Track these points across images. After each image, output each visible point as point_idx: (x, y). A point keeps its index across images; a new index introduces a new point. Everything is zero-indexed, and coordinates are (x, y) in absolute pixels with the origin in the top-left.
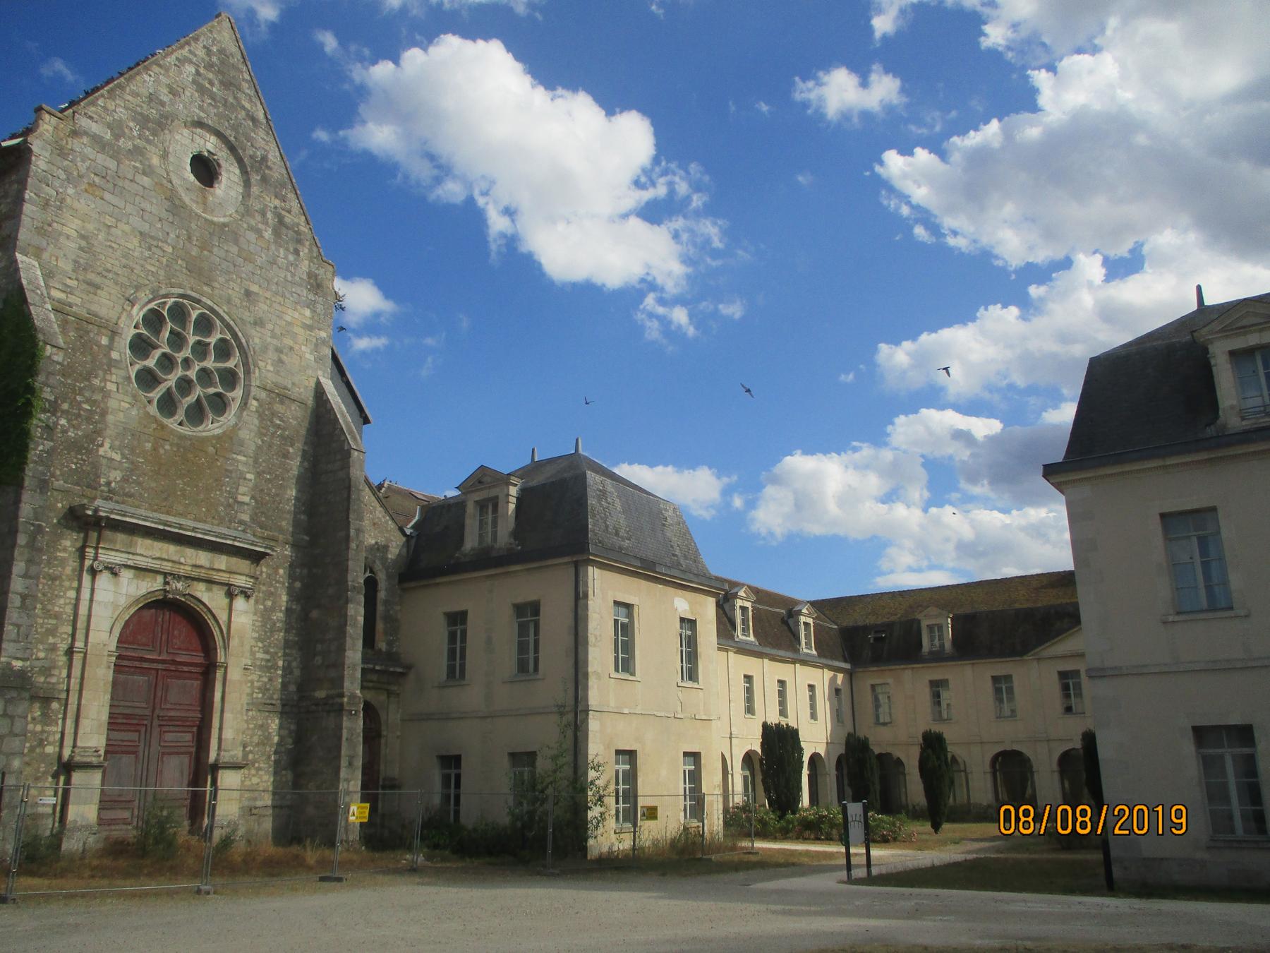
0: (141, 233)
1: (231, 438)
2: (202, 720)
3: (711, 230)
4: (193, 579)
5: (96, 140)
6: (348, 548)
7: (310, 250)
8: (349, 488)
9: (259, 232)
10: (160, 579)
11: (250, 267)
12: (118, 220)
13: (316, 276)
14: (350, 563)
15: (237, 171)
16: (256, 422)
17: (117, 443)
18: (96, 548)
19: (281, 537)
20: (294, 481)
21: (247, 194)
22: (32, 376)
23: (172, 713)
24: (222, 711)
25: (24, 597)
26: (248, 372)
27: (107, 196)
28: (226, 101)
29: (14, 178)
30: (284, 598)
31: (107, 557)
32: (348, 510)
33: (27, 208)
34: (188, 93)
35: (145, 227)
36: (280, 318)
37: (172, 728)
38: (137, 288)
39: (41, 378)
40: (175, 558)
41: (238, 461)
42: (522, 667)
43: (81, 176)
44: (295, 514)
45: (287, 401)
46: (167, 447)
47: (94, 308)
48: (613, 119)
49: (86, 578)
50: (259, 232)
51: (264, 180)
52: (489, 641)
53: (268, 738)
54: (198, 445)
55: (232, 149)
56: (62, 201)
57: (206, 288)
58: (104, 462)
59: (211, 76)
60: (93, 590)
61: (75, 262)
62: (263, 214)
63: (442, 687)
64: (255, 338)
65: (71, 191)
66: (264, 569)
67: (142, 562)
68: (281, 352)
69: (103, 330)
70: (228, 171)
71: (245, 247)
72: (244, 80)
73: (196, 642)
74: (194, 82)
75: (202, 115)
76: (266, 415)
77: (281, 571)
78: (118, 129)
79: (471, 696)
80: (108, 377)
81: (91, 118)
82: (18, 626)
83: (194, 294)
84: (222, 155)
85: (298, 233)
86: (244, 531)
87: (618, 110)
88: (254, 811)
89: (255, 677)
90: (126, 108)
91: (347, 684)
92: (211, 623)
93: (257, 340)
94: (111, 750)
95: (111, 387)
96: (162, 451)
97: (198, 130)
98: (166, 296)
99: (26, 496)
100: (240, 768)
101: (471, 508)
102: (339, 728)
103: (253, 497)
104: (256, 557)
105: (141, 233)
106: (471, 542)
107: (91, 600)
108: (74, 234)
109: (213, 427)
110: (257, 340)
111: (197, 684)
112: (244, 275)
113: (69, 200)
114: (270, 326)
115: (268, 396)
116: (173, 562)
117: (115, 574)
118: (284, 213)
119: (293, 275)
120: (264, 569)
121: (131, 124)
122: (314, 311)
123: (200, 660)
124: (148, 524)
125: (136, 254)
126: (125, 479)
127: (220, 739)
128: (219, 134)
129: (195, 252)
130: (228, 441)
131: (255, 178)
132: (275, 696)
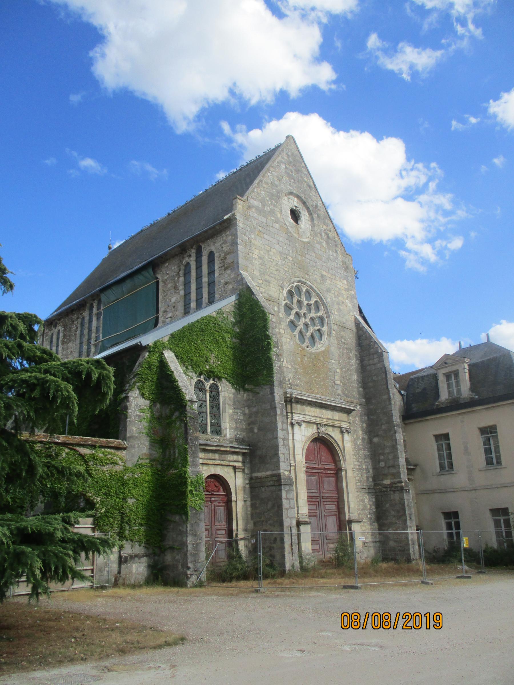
0: (280, 252)
1: (328, 352)
2: (339, 498)
3: (445, 201)
4: (327, 425)
5: (257, 208)
6: (390, 404)
7: (341, 249)
8: (386, 372)
9: (320, 244)
10: (315, 426)
11: (321, 263)
12: (271, 248)
13: (346, 262)
14: (393, 412)
15: (307, 214)
16: (336, 342)
17: (289, 359)
18: (292, 413)
19: (355, 401)
20: (354, 371)
21: (313, 226)
22: (267, 330)
23: (327, 495)
24: (348, 493)
25: (284, 440)
26: (328, 317)
27: (266, 236)
28: (298, 179)
29: (228, 233)
30: (361, 432)
31: (297, 417)
32: (387, 383)
33: (240, 247)
34: (284, 179)
35: (280, 249)
36: (336, 286)
37: (328, 503)
38: (283, 280)
39: (270, 331)
40: (320, 416)
41: (333, 363)
42: (489, 462)
43: (255, 228)
44: (358, 388)
45: (346, 330)
46: (306, 359)
47: (270, 293)
48: (381, 142)
49: (290, 428)
50: (320, 244)
51: (318, 216)
52: (466, 449)
53: (365, 506)
54: (316, 357)
55: (304, 203)
56: (251, 242)
57: (307, 276)
58: (286, 369)
59: (291, 168)
60: (293, 434)
61: (260, 271)
62: (321, 235)
63: (438, 475)
64: (329, 298)
65: (253, 236)
66: (351, 418)
67: (309, 419)
68: (339, 304)
69: (275, 303)
70: (304, 215)
71: (317, 252)
72: (302, 167)
73: (330, 459)
74: (286, 172)
75: (291, 188)
76: (340, 338)
77: (357, 419)
78: (263, 201)
79: (459, 479)
80: (280, 327)
81: (253, 198)
82: (284, 454)
83: (303, 280)
84: (301, 208)
85: (335, 241)
86: (341, 399)
87: (384, 137)
88: (366, 545)
89: (356, 475)
90: (264, 191)
91: (402, 476)
92: (337, 447)
93: (329, 300)
94: (311, 514)
95: (282, 331)
96: (304, 362)
97: (290, 196)
98: (293, 283)
99: (276, 390)
100: (360, 522)
101: (441, 379)
102: (402, 499)
103: (341, 381)
104: (348, 412)
105: (280, 252)
106: (444, 396)
107: (293, 439)
108: (257, 257)
109: (320, 347)
110: (329, 300)
111: (333, 479)
112: (319, 267)
113: (253, 241)
114: (333, 292)
115: (338, 328)
116: (320, 417)
117: (300, 425)
118: (329, 232)
119: (337, 263)
120: (351, 418)
121: (268, 199)
122: (347, 281)
123: (333, 467)
124: (310, 399)
125: (280, 263)
126: (294, 378)
127: (349, 508)
128: (298, 197)
129: (300, 258)
130: (326, 352)
131: (315, 216)
132: (365, 484)
